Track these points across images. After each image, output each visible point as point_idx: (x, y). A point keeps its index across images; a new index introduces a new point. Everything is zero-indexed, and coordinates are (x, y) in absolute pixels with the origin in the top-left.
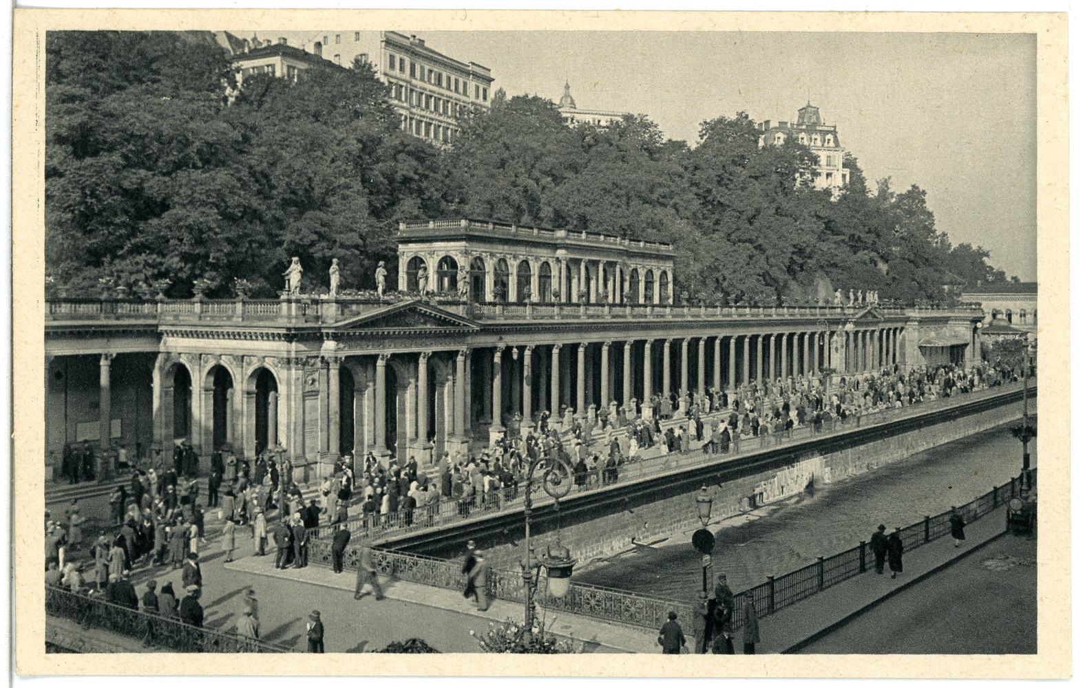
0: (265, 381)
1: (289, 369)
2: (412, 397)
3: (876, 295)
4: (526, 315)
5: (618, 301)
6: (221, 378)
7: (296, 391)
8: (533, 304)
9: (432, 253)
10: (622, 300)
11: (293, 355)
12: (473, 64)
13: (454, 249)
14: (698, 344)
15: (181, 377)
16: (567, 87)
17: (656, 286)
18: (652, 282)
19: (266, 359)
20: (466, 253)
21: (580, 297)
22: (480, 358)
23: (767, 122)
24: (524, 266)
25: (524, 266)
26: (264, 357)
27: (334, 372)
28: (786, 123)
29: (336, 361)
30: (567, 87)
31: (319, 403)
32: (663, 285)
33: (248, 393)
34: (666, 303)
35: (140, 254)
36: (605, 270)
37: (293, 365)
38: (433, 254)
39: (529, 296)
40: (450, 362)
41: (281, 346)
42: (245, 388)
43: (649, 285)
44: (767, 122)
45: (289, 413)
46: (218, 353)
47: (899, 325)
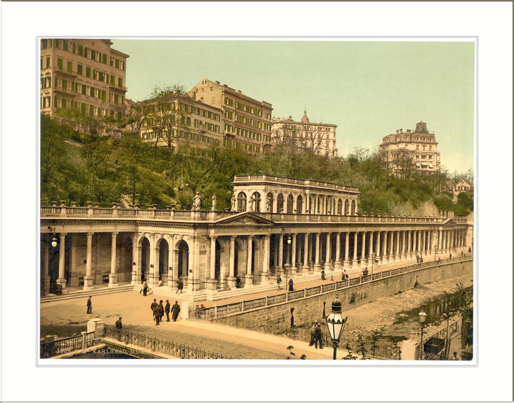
0: (183, 247)
1: (194, 242)
2: (247, 254)
3: (453, 214)
4: (295, 220)
5: (325, 214)
6: (163, 246)
7: (197, 250)
8: (284, 214)
9: (249, 190)
10: (326, 213)
11: (196, 235)
12: (264, 102)
13: (260, 189)
14: (370, 235)
15: (145, 243)
16: (305, 112)
17: (343, 207)
18: (348, 206)
19: (165, 235)
20: (265, 190)
21: (307, 211)
22: (274, 239)
23: (401, 130)
24: (291, 197)
25: (291, 197)
26: (183, 235)
27: (213, 243)
28: (410, 130)
29: (214, 238)
30: (305, 112)
31: (206, 257)
32: (353, 207)
33: (176, 251)
34: (347, 215)
35: (422, 190)
36: (318, 199)
37: (196, 240)
38: (249, 191)
39: (283, 210)
40: (261, 240)
41: (191, 232)
42: (174, 249)
43: (347, 206)
44: (401, 130)
45: (194, 261)
46: (172, 233)
47: (463, 227)
